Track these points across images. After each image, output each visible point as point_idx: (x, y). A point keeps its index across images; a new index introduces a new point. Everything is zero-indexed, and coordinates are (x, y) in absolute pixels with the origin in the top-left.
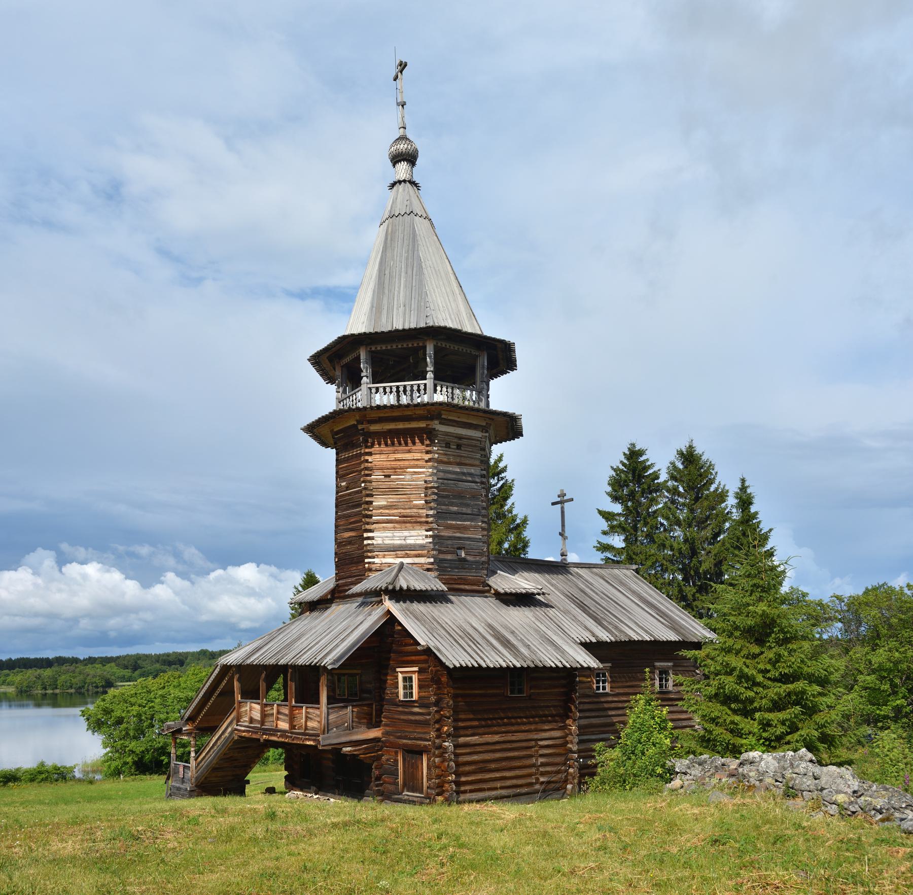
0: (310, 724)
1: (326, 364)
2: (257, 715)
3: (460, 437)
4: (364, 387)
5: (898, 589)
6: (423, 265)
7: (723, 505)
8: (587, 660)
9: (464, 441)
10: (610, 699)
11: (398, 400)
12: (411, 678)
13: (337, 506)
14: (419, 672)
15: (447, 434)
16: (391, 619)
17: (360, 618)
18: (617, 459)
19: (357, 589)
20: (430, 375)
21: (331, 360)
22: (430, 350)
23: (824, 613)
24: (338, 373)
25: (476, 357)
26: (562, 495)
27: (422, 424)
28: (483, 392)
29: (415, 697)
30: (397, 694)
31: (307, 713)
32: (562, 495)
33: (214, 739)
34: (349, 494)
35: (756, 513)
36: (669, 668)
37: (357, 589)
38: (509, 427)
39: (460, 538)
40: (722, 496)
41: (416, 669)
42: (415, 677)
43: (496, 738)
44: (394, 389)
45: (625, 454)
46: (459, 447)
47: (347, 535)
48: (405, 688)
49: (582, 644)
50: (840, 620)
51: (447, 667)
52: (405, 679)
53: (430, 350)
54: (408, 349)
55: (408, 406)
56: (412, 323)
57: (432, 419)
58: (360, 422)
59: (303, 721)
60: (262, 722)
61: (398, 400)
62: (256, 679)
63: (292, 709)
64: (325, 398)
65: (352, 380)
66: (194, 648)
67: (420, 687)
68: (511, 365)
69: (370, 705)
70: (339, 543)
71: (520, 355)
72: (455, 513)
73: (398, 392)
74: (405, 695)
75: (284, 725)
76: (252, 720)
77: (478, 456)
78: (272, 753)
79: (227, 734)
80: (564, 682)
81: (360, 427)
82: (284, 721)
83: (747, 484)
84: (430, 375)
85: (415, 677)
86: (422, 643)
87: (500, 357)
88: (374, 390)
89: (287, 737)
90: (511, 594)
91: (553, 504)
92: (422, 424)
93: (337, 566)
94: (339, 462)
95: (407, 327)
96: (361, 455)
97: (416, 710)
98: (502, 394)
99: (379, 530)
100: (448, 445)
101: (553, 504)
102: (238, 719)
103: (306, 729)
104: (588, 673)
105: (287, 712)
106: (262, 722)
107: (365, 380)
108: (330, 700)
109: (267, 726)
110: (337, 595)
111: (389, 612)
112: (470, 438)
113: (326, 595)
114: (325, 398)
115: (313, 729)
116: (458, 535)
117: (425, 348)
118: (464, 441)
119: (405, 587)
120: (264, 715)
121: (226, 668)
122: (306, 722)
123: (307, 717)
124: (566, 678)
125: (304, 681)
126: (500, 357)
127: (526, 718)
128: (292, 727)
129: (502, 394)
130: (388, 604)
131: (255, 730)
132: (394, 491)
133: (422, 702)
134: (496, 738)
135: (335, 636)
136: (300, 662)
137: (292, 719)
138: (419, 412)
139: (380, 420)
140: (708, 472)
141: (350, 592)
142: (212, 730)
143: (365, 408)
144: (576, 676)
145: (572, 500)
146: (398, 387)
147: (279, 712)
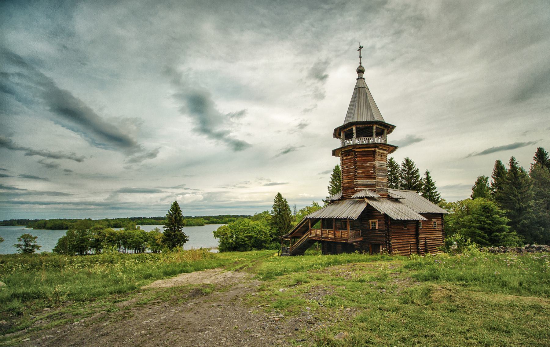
5: (337, 161)
6: (342, 257)
7: (420, 178)
12: (375, 223)
17: (16, 80)
20: (374, 135)
22: (374, 128)
23: (541, 261)
27: (373, 149)
35: (335, 153)
40: (417, 171)
43: (401, 241)
45: (330, 182)
50: (277, 320)
52: (372, 223)
53: (354, 128)
56: (369, 119)
60: (322, 235)
62: (328, 223)
63: (334, 231)
64: (337, 143)
67: (379, 226)
72: (24, 329)
78: (316, 243)
83: (430, 175)
87: (390, 128)
92: (373, 149)
96: (508, 179)
106: (322, 235)
109: (323, 236)
114: (337, 143)
120: (322, 233)
124: (416, 223)
125: (342, 223)
126: (390, 128)
128: (335, 236)
130: (366, 200)
132: (363, 168)
134: (401, 241)
137: (334, 234)
139: (360, 148)
140: (412, 165)
141: (353, 197)
145: (427, 173)
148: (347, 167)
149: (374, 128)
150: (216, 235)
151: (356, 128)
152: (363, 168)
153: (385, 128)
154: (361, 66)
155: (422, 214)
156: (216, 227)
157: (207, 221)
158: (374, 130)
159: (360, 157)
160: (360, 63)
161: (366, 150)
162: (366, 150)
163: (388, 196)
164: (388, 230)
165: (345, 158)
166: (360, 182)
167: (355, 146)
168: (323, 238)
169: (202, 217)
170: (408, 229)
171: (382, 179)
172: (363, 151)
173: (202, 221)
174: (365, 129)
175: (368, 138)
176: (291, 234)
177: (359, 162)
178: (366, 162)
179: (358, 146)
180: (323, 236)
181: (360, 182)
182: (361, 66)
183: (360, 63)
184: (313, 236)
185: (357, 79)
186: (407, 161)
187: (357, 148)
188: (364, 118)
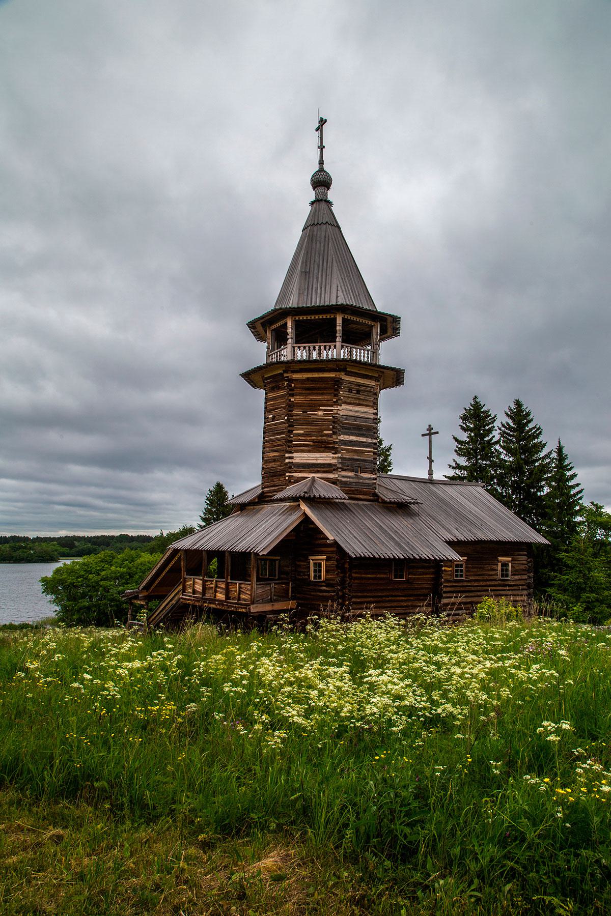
0: (242, 596)
1: (260, 328)
2: (199, 588)
3: (359, 385)
4: (289, 346)
8: (452, 555)
9: (362, 388)
10: (465, 584)
11: (320, 356)
13: (264, 433)
14: (327, 560)
15: (350, 382)
16: (306, 520)
18: (468, 404)
19: (280, 495)
20: (339, 339)
21: (263, 325)
22: (339, 321)
24: (269, 335)
25: (372, 326)
26: (430, 428)
27: (332, 375)
28: (375, 353)
29: (323, 578)
30: (309, 576)
31: (240, 587)
32: (430, 428)
33: (164, 605)
34: (275, 425)
36: (509, 561)
37: (280, 495)
38: (395, 377)
39: (357, 460)
40: (538, 432)
41: (324, 557)
42: (323, 564)
44: (317, 348)
46: (358, 392)
47: (272, 454)
48: (315, 571)
49: (446, 542)
51: (350, 557)
52: (315, 564)
53: (289, 324)
54: (323, 319)
55: (315, 361)
57: (340, 371)
58: (285, 371)
59: (236, 594)
60: (204, 593)
61: (320, 356)
62: (196, 561)
63: (227, 585)
64: (259, 353)
65: (280, 339)
66: (116, 533)
67: (327, 571)
68: (396, 332)
69: (287, 584)
70: (265, 461)
71: (403, 326)
73: (320, 350)
74: (315, 577)
75: (221, 596)
76: (194, 592)
77: (372, 399)
79: (174, 602)
80: (432, 570)
81: (285, 375)
82: (221, 593)
84: (339, 339)
85: (323, 564)
86: (331, 538)
87: (389, 325)
88: (312, 348)
89: (223, 605)
90: (394, 503)
91: (423, 435)
92: (332, 375)
93: (263, 478)
94: (267, 400)
95: (300, 306)
97: (324, 588)
98: (388, 353)
99: (297, 451)
100: (350, 391)
101: (423, 435)
102: (184, 590)
103: (239, 599)
104: (449, 564)
105: (224, 586)
107: (290, 341)
108: (258, 580)
110: (262, 499)
111: (304, 513)
112: (366, 386)
113: (255, 499)
114: (259, 353)
115: (245, 600)
116: (356, 457)
117: (335, 319)
118: (362, 388)
119: (317, 496)
121: (176, 551)
122: (239, 594)
123: (240, 591)
125: (236, 564)
126: (389, 325)
127: (21, 547)
128: (228, 597)
129: (388, 353)
130: (304, 507)
131: (198, 600)
132: (309, 422)
133: (328, 583)
135: (261, 533)
136: (237, 549)
137: (227, 592)
138: (331, 366)
141: (275, 497)
142: (162, 598)
143: (288, 362)
144: (442, 566)
146: (320, 347)
147: (216, 586)
148: (274, 419)
149: (339, 321)
150: (50, 586)
151: (344, 319)
152: (309, 422)
153: (379, 325)
154: (321, 170)
155: (450, 543)
156: (49, 570)
157: (65, 550)
158: (339, 328)
159: (300, 394)
160: (321, 163)
161: (316, 375)
162: (316, 375)
163: (375, 495)
164: (342, 583)
165: (271, 395)
166: (299, 457)
167: (293, 366)
168: (205, 600)
169: (54, 539)
170: (408, 581)
171: (356, 451)
172: (308, 379)
173: (49, 547)
174: (314, 324)
175: (317, 345)
176: (146, 588)
177: (299, 406)
178: (315, 406)
179: (297, 367)
180: (208, 596)
181: (299, 457)
182: (321, 170)
183: (321, 163)
184: (188, 596)
185: (312, 203)
186: (518, 404)
187: (294, 372)
188: (335, 294)
